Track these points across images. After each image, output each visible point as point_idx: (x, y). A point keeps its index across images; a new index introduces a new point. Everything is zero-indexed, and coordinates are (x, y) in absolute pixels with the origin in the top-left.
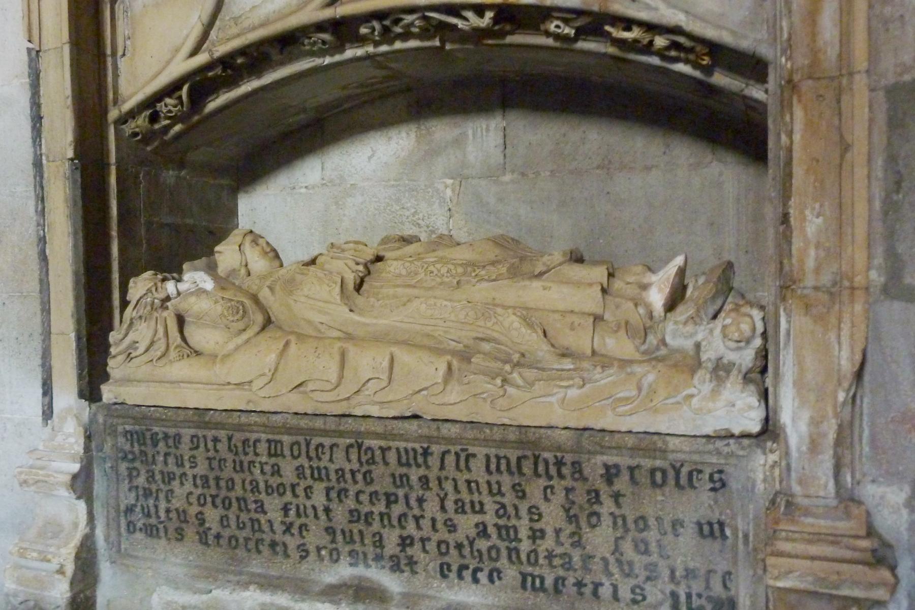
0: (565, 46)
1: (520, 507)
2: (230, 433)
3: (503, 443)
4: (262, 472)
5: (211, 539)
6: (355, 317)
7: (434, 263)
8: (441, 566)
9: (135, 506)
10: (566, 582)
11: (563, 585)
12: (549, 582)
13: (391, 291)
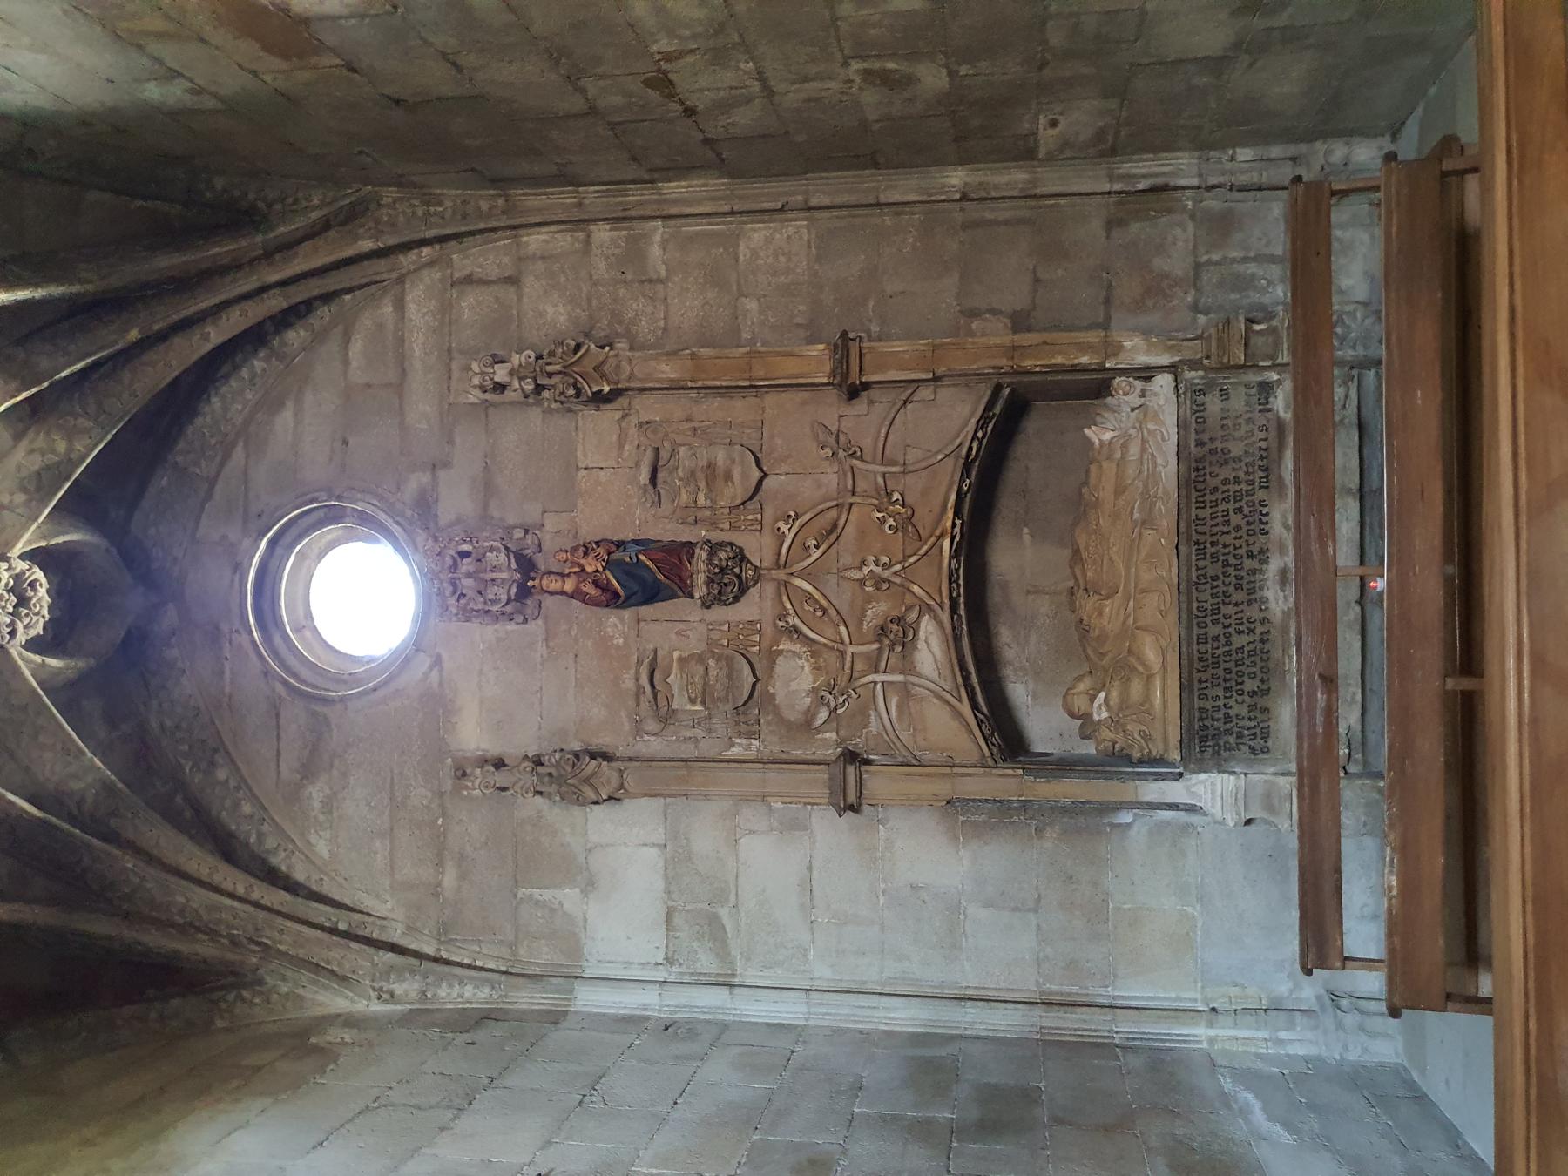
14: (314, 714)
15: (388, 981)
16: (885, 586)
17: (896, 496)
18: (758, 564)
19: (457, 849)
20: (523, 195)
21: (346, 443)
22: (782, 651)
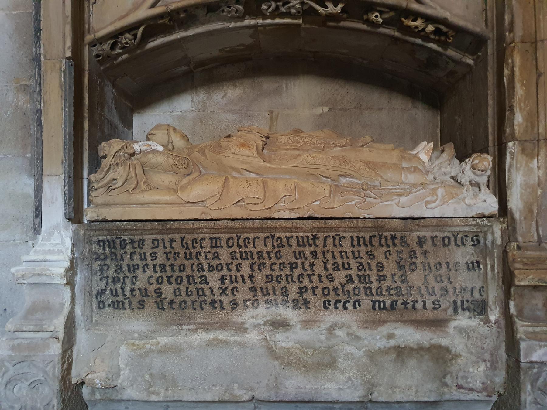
0: (373, 30)
1: (371, 264)
2: (183, 236)
3: (364, 228)
4: (206, 258)
5: (166, 305)
6: (265, 164)
8: (324, 302)
9: (105, 290)
10: (398, 303)
11: (396, 305)
12: (388, 304)
13: (283, 152)
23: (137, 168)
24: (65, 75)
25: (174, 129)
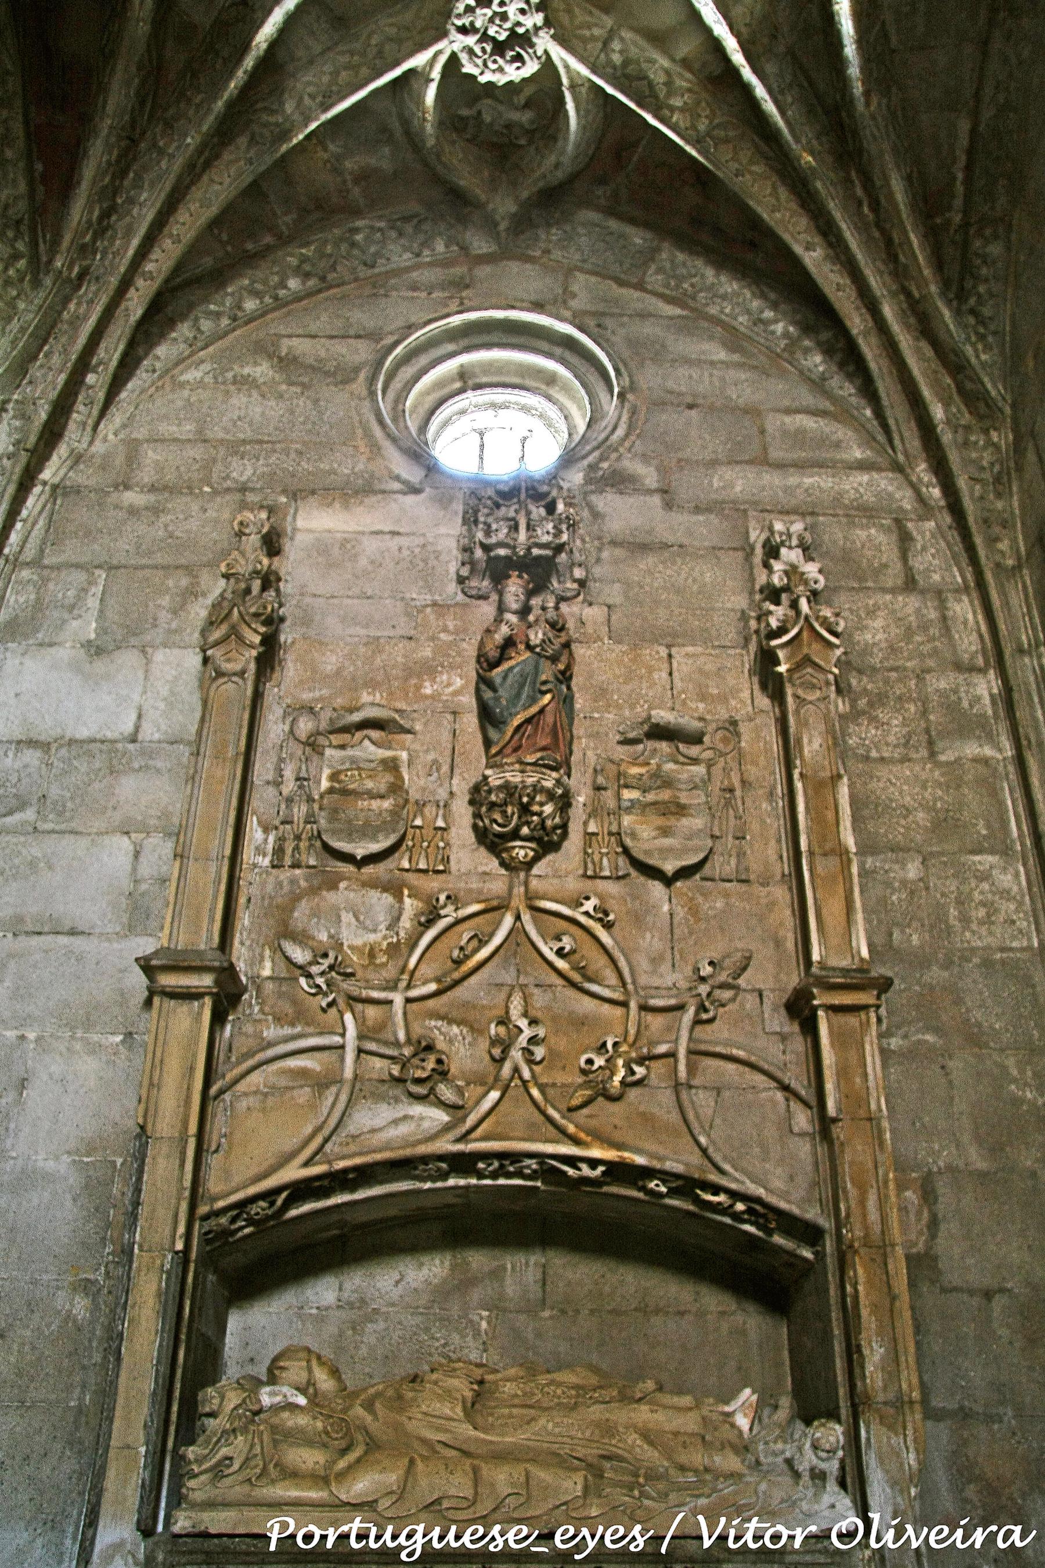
0: (653, 1200)
7: (547, 1385)
13: (507, 1411)
14: (357, 370)
15: (14, 417)
16: (497, 1052)
17: (640, 1071)
18: (535, 871)
19: (170, 506)
20: (1025, 587)
21: (690, 407)
22: (401, 901)
23: (265, 1437)
24: (168, 1279)
25: (319, 1358)
